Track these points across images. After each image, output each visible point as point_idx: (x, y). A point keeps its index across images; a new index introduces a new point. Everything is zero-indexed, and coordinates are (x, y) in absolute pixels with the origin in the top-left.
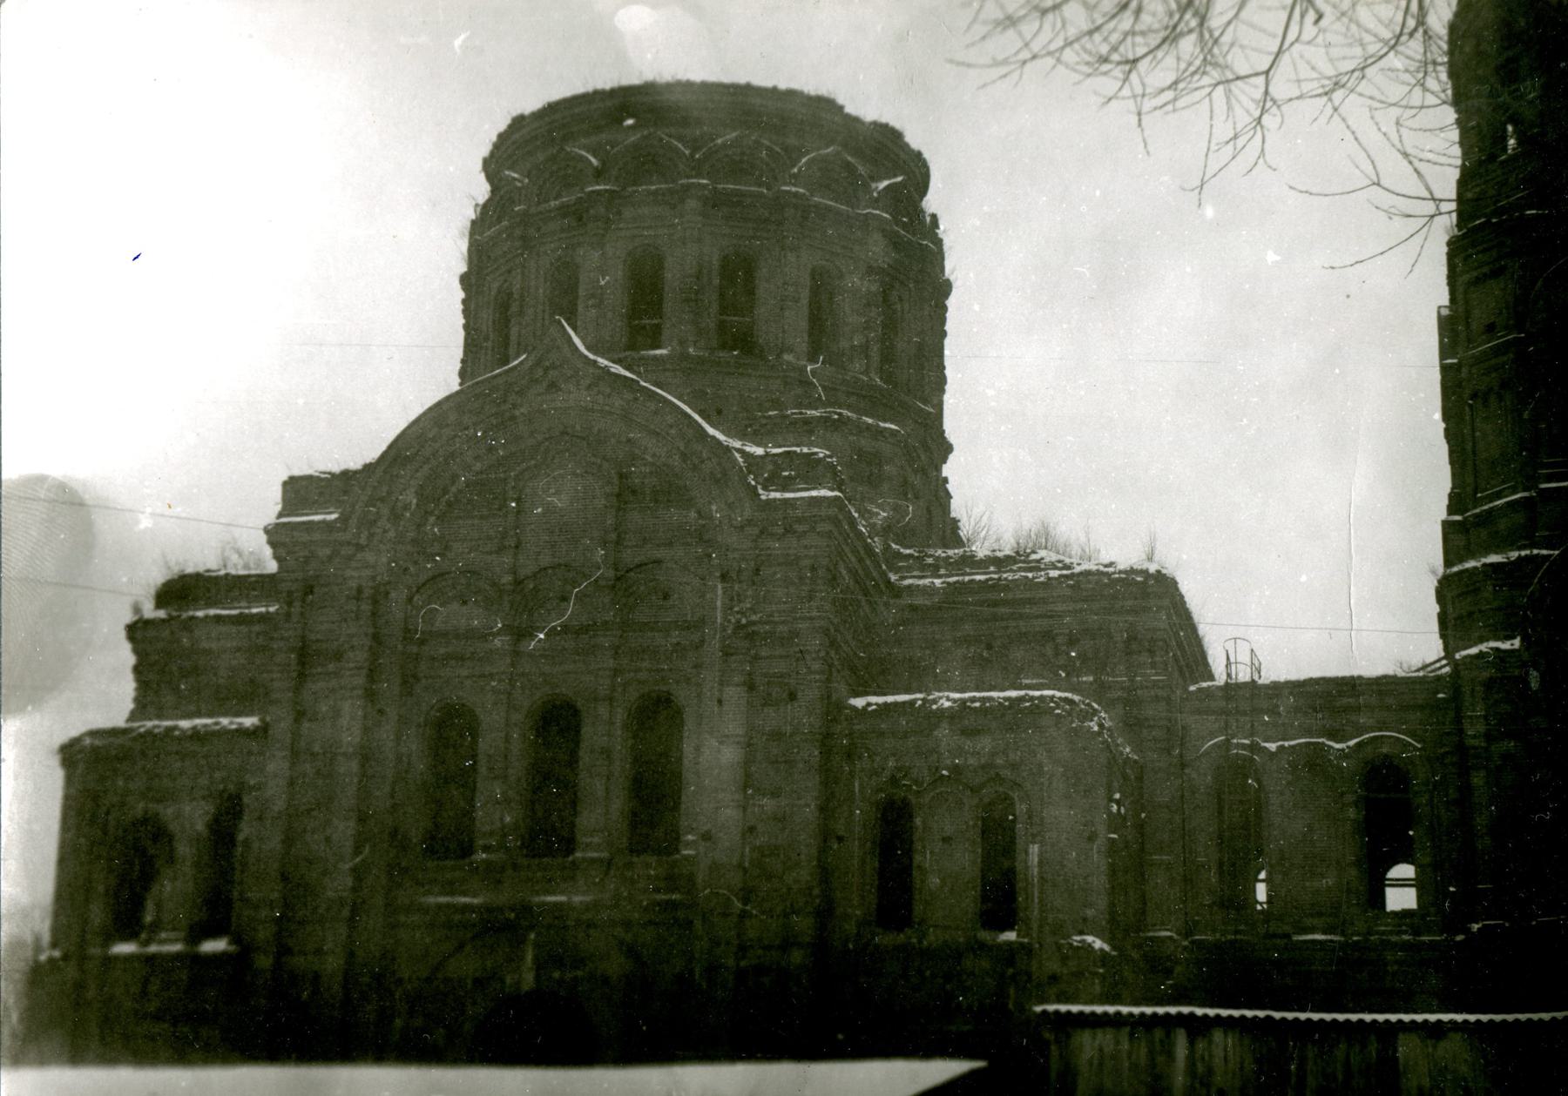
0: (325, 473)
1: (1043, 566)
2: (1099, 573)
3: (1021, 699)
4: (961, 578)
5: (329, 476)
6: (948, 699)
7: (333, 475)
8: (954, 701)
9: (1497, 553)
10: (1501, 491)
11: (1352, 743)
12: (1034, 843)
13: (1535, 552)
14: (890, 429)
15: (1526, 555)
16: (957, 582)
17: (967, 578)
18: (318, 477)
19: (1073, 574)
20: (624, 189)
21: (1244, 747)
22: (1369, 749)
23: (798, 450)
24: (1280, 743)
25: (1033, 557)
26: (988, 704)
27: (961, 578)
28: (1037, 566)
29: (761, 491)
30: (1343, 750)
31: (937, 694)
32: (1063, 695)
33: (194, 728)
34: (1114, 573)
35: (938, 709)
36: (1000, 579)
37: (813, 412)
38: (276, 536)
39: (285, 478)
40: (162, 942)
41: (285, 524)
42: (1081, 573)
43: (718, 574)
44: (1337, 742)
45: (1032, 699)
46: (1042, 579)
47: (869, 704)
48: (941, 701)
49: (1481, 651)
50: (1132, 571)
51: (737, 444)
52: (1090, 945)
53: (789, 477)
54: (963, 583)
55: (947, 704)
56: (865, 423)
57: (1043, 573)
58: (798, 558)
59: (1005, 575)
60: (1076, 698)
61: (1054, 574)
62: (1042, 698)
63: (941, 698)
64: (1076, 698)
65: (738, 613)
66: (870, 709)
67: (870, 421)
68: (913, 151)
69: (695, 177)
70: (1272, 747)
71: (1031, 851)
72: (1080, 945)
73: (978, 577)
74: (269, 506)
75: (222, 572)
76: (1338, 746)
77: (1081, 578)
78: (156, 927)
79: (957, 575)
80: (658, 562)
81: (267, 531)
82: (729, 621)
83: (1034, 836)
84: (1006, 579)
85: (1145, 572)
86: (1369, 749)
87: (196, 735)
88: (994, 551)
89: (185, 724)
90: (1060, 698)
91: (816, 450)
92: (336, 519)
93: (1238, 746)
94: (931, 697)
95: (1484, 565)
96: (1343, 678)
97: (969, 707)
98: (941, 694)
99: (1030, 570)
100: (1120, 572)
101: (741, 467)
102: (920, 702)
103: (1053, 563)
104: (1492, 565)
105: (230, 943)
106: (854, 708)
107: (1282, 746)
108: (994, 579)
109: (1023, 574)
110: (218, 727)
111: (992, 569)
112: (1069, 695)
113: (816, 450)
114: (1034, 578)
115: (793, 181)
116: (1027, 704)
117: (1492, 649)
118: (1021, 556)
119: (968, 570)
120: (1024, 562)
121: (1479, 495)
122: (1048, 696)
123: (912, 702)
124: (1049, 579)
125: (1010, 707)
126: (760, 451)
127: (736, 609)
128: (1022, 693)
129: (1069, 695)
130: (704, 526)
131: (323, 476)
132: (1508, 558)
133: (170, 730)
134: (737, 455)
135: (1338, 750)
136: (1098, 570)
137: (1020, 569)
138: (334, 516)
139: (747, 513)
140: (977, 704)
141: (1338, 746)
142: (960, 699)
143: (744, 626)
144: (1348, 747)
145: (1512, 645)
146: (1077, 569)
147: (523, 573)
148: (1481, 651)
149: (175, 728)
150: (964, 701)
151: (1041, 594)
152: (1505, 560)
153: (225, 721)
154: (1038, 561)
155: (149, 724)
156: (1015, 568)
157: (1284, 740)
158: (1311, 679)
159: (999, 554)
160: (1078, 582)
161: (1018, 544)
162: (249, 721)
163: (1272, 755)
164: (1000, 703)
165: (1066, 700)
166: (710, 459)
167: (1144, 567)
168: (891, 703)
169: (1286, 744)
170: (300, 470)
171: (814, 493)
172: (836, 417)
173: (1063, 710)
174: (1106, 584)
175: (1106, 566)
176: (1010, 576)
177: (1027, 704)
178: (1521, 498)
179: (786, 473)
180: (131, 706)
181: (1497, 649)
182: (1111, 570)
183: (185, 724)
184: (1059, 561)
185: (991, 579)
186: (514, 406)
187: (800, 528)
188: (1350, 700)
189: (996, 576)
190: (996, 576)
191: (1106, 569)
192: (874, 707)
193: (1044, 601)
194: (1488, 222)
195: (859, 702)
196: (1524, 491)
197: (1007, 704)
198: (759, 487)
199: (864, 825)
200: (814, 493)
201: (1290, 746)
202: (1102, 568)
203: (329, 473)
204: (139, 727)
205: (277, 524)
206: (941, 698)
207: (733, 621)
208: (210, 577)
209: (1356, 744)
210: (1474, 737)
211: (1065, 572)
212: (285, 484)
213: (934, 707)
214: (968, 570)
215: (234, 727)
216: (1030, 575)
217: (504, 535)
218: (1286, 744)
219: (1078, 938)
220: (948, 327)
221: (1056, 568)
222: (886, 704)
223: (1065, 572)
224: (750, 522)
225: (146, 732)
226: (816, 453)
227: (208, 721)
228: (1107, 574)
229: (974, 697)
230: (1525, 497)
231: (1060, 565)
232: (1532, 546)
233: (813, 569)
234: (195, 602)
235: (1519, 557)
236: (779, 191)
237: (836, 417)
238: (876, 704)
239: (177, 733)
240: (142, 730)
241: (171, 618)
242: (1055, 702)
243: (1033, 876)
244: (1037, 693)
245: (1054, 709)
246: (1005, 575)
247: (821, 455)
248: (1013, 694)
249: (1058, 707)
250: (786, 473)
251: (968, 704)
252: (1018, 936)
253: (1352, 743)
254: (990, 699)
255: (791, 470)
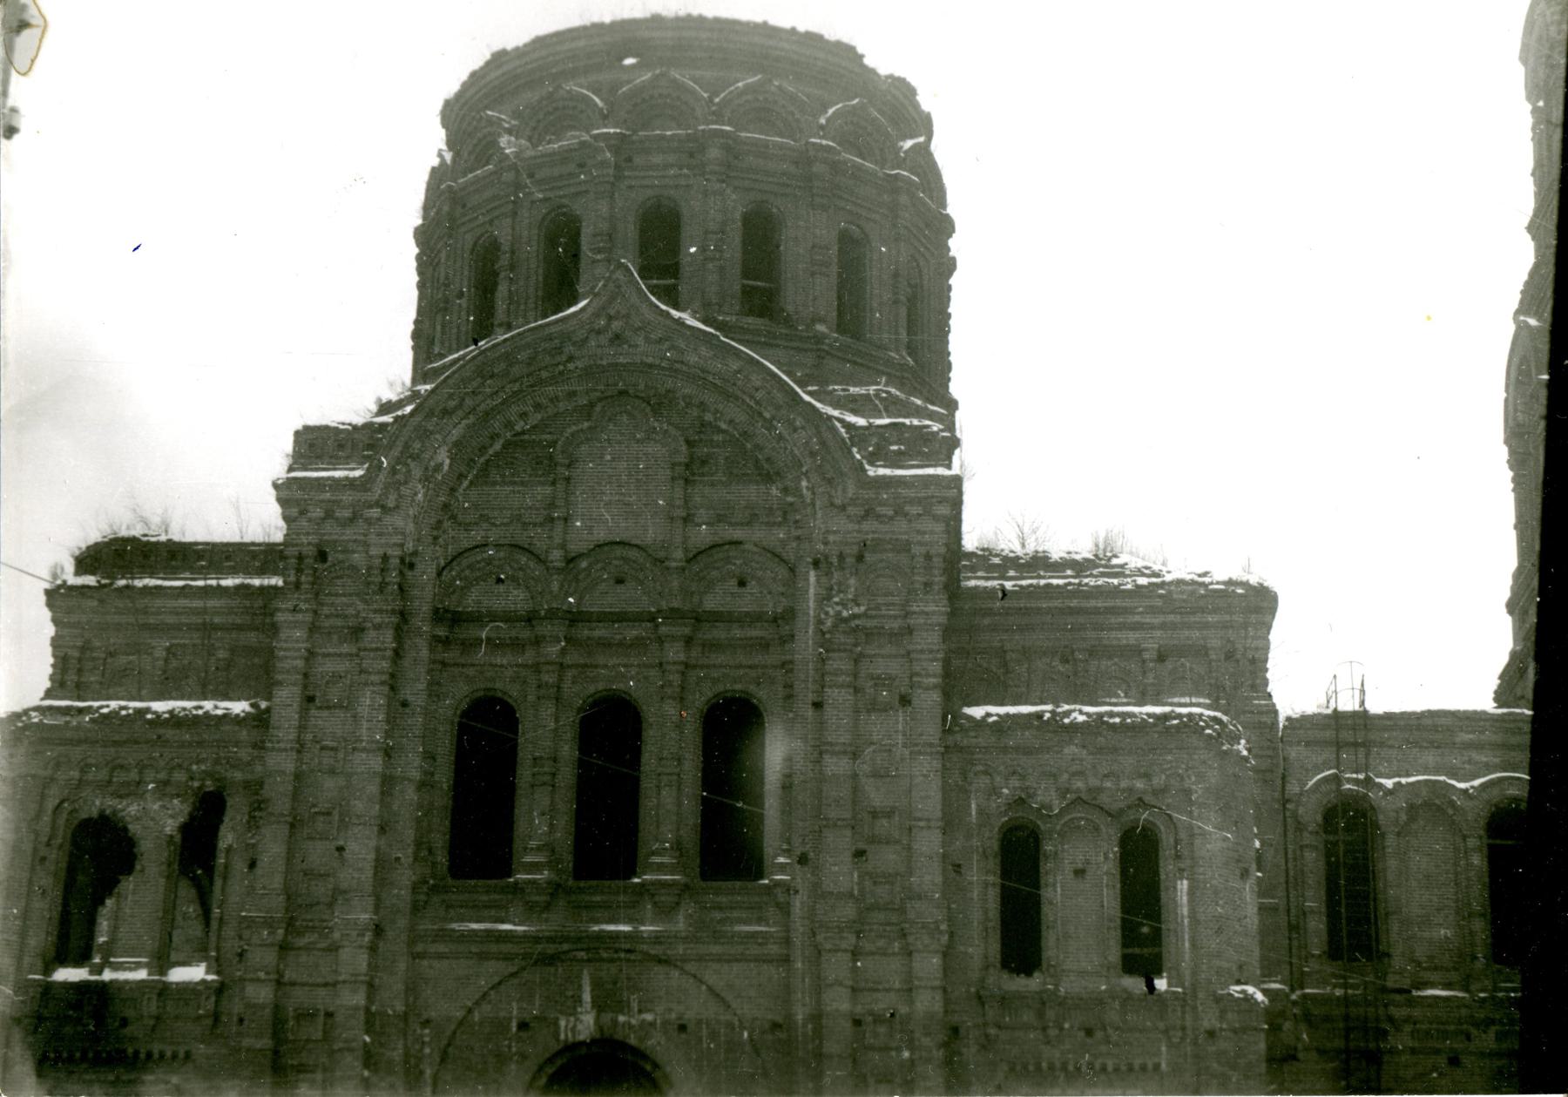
0: (343, 424)
1: (1128, 572)
2: (1193, 582)
4: (1034, 582)
5: (350, 428)
6: (1081, 712)
7: (355, 427)
8: (1088, 714)
11: (1477, 783)
14: (938, 413)
16: (1031, 585)
17: (1043, 582)
18: (337, 428)
19: (1163, 583)
20: (635, 132)
21: (1356, 782)
22: (1495, 791)
23: (907, 421)
24: (1396, 780)
25: (1115, 561)
26: (1129, 721)
27: (1034, 582)
28: (1120, 571)
29: (867, 467)
31: (1066, 707)
32: (1212, 713)
33: (171, 712)
34: (1212, 583)
35: (1071, 722)
36: (1080, 584)
37: (857, 389)
38: (290, 494)
39: (299, 426)
40: (117, 967)
41: (295, 479)
42: (1171, 583)
43: (809, 560)
45: (1180, 716)
46: (1129, 587)
47: (988, 715)
48: (1074, 715)
50: (1230, 582)
51: (836, 413)
52: (1252, 996)
53: (899, 453)
54: (1037, 587)
55: (1081, 718)
56: (913, 404)
57: (1129, 580)
58: (908, 543)
59: (1086, 581)
60: (1225, 718)
61: (1142, 581)
62: (1190, 715)
63: (1074, 711)
64: (1225, 718)
65: (837, 604)
66: (991, 720)
67: (919, 402)
68: (923, 111)
69: (716, 123)
70: (1389, 783)
71: (1179, 887)
72: (1241, 996)
73: (1055, 582)
74: (275, 459)
75: (163, 538)
76: (1462, 785)
77: (1173, 588)
78: (108, 951)
79: (1032, 578)
80: (738, 543)
81: (275, 486)
82: (827, 613)
83: (1181, 870)
84: (1087, 584)
87: (175, 720)
88: (1069, 553)
89: (160, 706)
90: (1209, 717)
91: (927, 422)
92: (361, 477)
93: (1349, 780)
94: (1060, 710)
97: (1107, 723)
98: (1072, 707)
99: (1115, 575)
101: (843, 440)
102: (1047, 715)
103: (1139, 570)
105: (208, 972)
106: (970, 718)
108: (1074, 584)
109: (1106, 580)
110: (200, 712)
111: (1069, 572)
112: (1218, 714)
113: (927, 422)
114: (1120, 585)
115: (821, 133)
116: (1175, 722)
118: (1101, 559)
119: (1042, 573)
120: (1106, 566)
123: (1039, 716)
124: (1138, 586)
126: (861, 422)
127: (836, 600)
128: (1167, 709)
129: (1218, 714)
130: (791, 504)
131: (341, 427)
133: (140, 712)
134: (838, 425)
135: (1461, 790)
136: (1192, 580)
137: (1103, 575)
138: (358, 473)
139: (851, 492)
140: (1117, 720)
141: (1462, 785)
142: (1097, 714)
143: (846, 620)
144: (1472, 787)
146: (1168, 578)
147: (574, 548)
149: (148, 710)
150: (1101, 715)
151: (1127, 603)
153: (208, 705)
154: (1122, 566)
155: (114, 704)
156: (1095, 572)
157: (1400, 776)
158: (1429, 712)
159: (1078, 557)
160: (1170, 592)
161: (1097, 546)
162: (239, 707)
163: (1389, 792)
164: (1142, 719)
165: (1215, 719)
166: (803, 428)
167: (1244, 579)
168: (1014, 715)
169: (1404, 781)
170: (314, 420)
171: (930, 471)
172: (884, 395)
173: (1214, 730)
174: (1203, 596)
175: (1200, 576)
176: (1092, 582)
177: (1175, 722)
179: (895, 448)
180: (48, 684)
182: (1207, 580)
183: (160, 706)
184: (1147, 568)
185: (1070, 584)
186: (571, 359)
187: (914, 510)
189: (1077, 581)
190: (1077, 581)
191: (1201, 580)
192: (995, 718)
195: (977, 712)
197: (1151, 720)
198: (864, 462)
199: (984, 852)
200: (930, 471)
201: (1408, 784)
202: (1196, 578)
203: (350, 424)
204: (102, 707)
205: (288, 478)
206: (1074, 711)
207: (832, 612)
208: (148, 543)
209: (1482, 785)
211: (1154, 580)
212: (297, 433)
213: (1066, 721)
214: (1042, 573)
215: (219, 712)
216: (1115, 581)
217: (552, 505)
218: (1404, 781)
219: (1238, 988)
221: (1143, 575)
222: (1007, 715)
223: (1154, 580)
224: (853, 501)
225: (110, 712)
226: (928, 426)
227: (188, 704)
229: (1112, 711)
231: (1147, 572)
233: (928, 557)
234: (128, 570)
236: (807, 143)
237: (884, 395)
238: (997, 715)
239: (149, 716)
240: (105, 711)
241: (102, 586)
242: (1205, 721)
243: (1182, 917)
244: (1184, 710)
246: (1086, 581)
247: (935, 429)
248: (1158, 710)
249: (1208, 726)
250: (895, 448)
251: (1105, 719)
252: (1170, 985)
253: (1477, 783)
255: (901, 444)
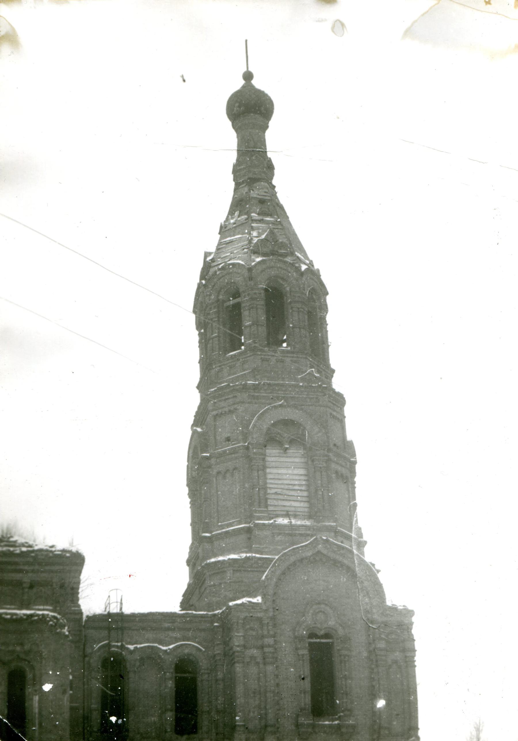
2: (47, 551)
3: (32, 616)
9: (235, 554)
10: (233, 522)
11: (171, 647)
12: (36, 695)
13: (254, 555)
15: (250, 556)
21: (117, 647)
24: (135, 646)
30: (166, 651)
44: (163, 646)
45: (38, 615)
49: (243, 602)
60: (59, 617)
61: (24, 549)
62: (43, 615)
64: (59, 617)
70: (131, 647)
85: (70, 552)
86: (179, 650)
95: (229, 559)
96: (167, 613)
100: (58, 551)
104: (232, 559)
107: (136, 648)
117: (248, 601)
121: (220, 524)
122: (46, 614)
125: (26, 619)
132: (240, 557)
140: (9, 617)
145: (258, 600)
148: (243, 602)
151: (16, 560)
152: (239, 558)
157: (137, 644)
173: (54, 622)
178: (244, 527)
181: (250, 602)
182: (53, 549)
188: (169, 625)
191: (51, 549)
193: (16, 564)
194: (229, 385)
196: (245, 523)
210: (238, 646)
218: (139, 646)
220: (193, 418)
228: (51, 551)
230: (247, 527)
231: (26, 545)
232: (250, 551)
235: (246, 557)
244: (40, 613)
245: (49, 621)
253: (171, 647)
254: (16, 614)
